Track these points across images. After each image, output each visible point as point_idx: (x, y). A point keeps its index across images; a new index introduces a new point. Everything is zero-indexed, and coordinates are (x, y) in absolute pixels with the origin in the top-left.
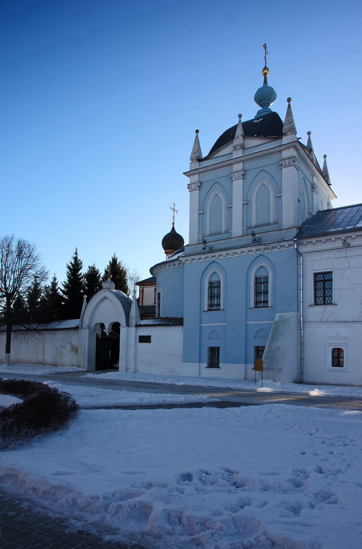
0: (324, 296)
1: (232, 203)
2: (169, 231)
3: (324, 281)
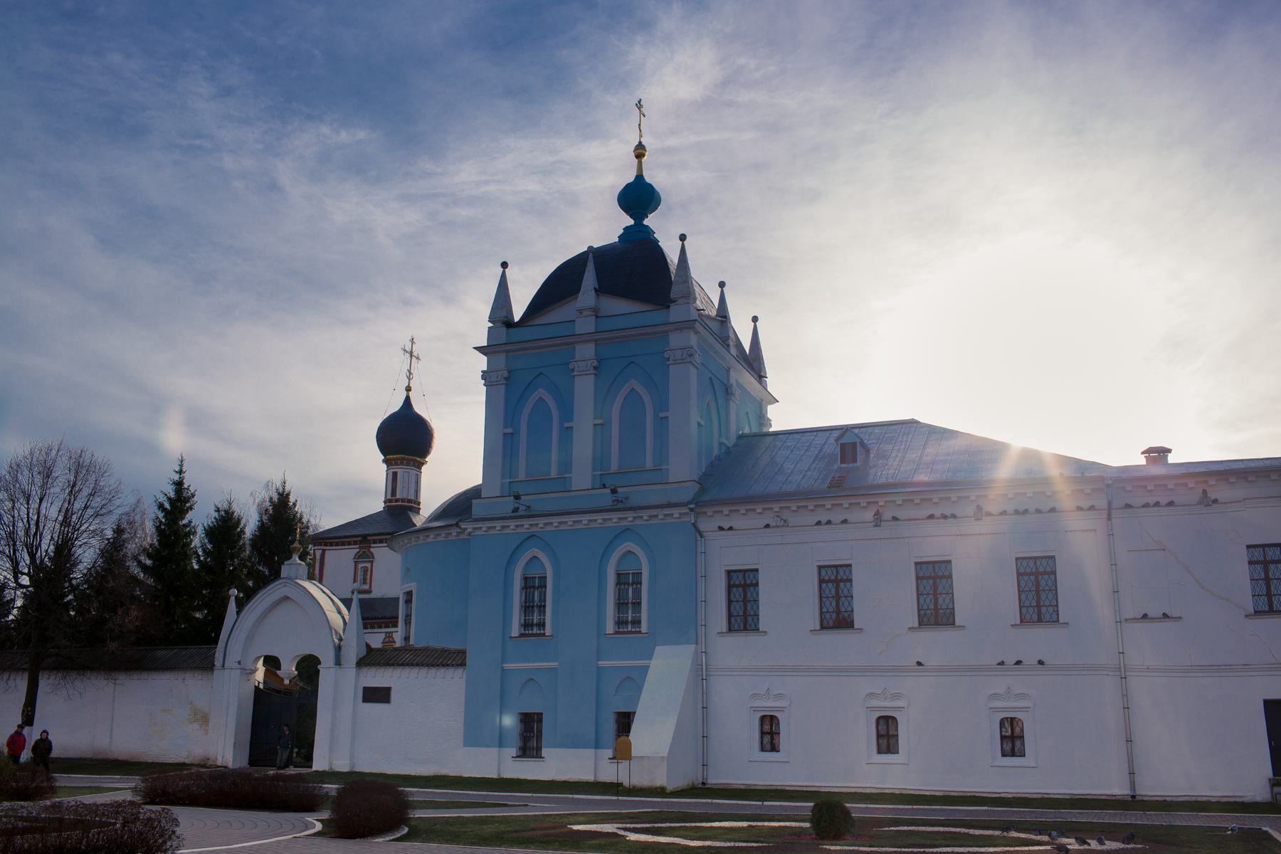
0: (745, 616)
1: (572, 420)
2: (396, 405)
3: (745, 586)
